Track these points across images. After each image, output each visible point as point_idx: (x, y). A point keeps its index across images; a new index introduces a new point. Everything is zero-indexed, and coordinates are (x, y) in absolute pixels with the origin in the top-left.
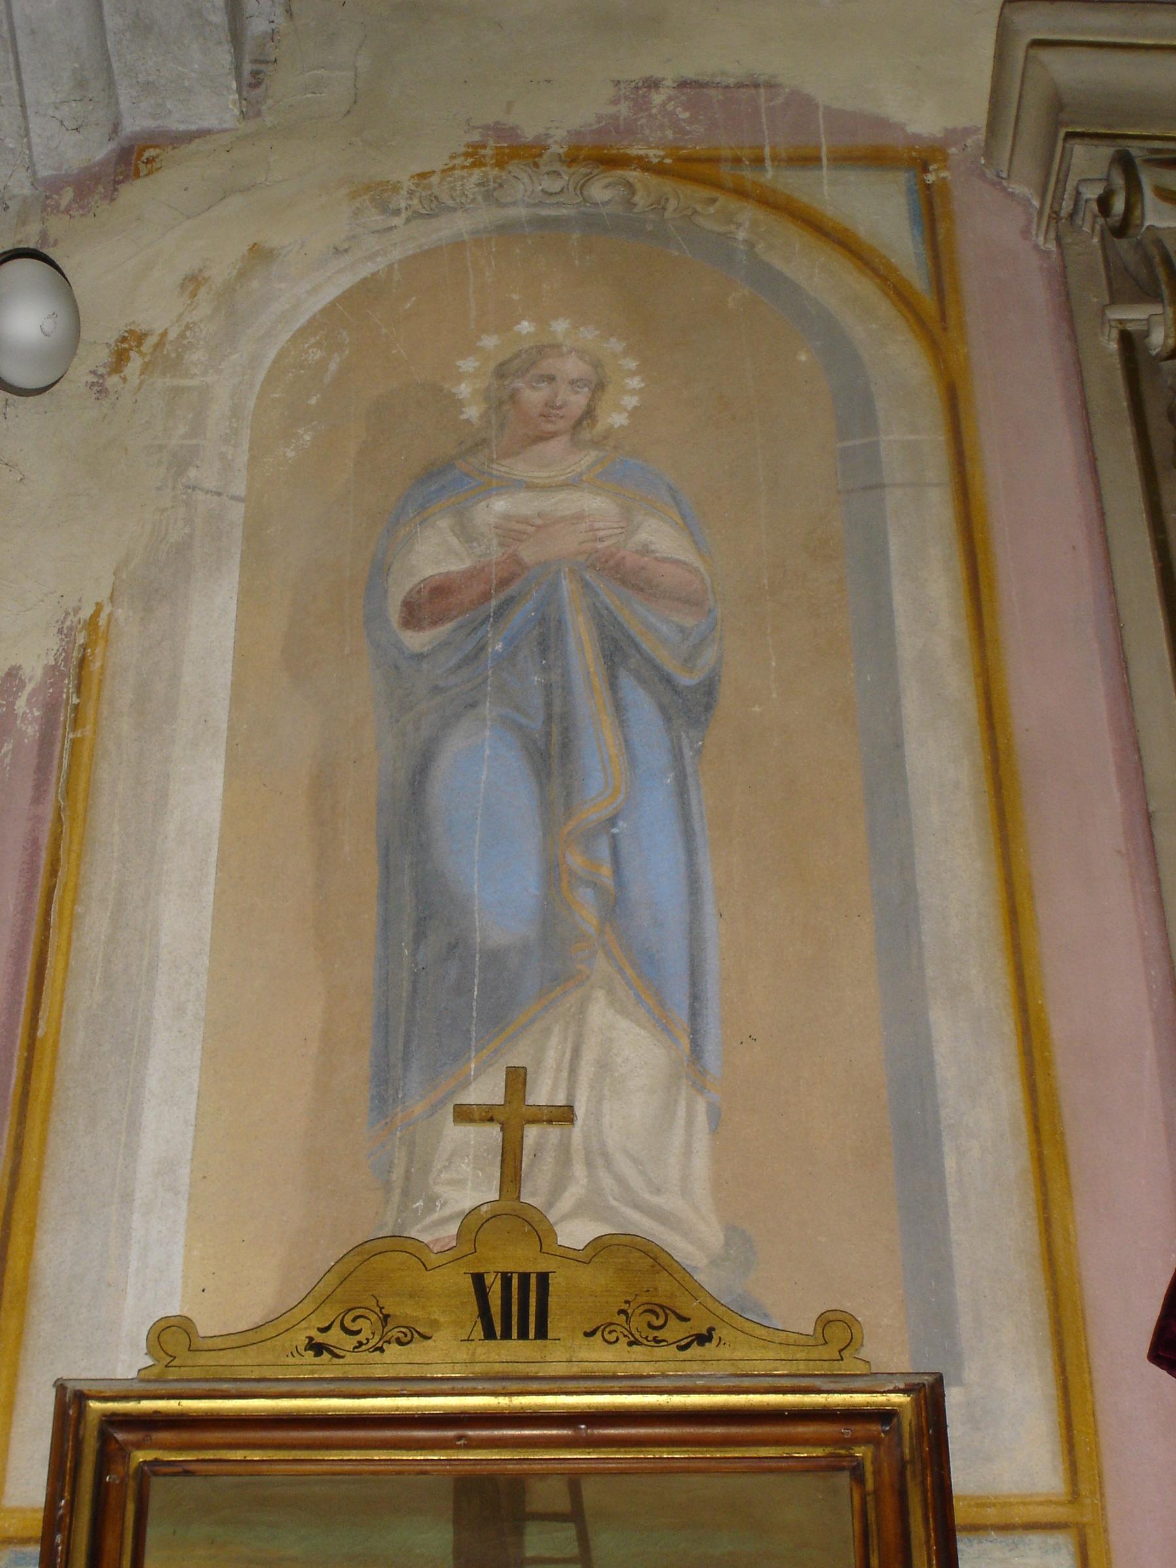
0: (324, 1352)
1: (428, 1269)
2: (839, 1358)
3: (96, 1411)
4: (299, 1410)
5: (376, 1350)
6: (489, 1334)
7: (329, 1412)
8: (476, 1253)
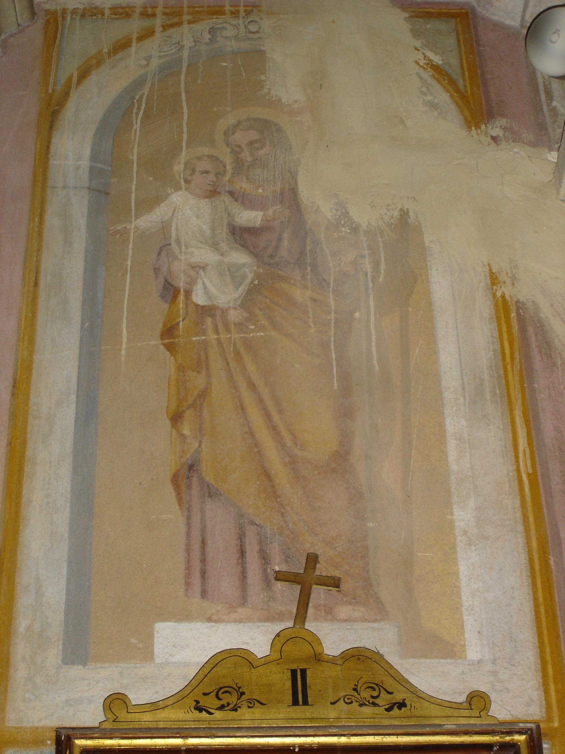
0: (203, 711)
1: (254, 667)
2: (479, 716)
3: (80, 746)
4: (243, 744)
5: (233, 710)
6: (295, 702)
7: (313, 744)
8: (282, 659)
